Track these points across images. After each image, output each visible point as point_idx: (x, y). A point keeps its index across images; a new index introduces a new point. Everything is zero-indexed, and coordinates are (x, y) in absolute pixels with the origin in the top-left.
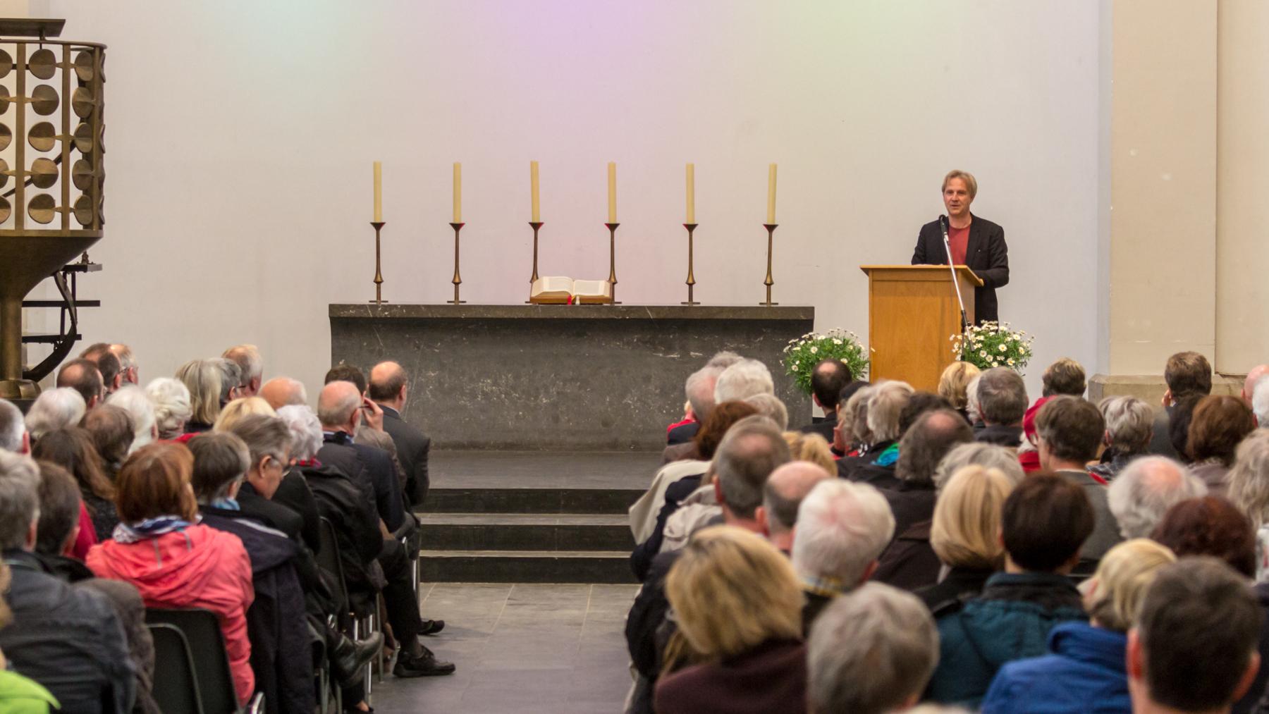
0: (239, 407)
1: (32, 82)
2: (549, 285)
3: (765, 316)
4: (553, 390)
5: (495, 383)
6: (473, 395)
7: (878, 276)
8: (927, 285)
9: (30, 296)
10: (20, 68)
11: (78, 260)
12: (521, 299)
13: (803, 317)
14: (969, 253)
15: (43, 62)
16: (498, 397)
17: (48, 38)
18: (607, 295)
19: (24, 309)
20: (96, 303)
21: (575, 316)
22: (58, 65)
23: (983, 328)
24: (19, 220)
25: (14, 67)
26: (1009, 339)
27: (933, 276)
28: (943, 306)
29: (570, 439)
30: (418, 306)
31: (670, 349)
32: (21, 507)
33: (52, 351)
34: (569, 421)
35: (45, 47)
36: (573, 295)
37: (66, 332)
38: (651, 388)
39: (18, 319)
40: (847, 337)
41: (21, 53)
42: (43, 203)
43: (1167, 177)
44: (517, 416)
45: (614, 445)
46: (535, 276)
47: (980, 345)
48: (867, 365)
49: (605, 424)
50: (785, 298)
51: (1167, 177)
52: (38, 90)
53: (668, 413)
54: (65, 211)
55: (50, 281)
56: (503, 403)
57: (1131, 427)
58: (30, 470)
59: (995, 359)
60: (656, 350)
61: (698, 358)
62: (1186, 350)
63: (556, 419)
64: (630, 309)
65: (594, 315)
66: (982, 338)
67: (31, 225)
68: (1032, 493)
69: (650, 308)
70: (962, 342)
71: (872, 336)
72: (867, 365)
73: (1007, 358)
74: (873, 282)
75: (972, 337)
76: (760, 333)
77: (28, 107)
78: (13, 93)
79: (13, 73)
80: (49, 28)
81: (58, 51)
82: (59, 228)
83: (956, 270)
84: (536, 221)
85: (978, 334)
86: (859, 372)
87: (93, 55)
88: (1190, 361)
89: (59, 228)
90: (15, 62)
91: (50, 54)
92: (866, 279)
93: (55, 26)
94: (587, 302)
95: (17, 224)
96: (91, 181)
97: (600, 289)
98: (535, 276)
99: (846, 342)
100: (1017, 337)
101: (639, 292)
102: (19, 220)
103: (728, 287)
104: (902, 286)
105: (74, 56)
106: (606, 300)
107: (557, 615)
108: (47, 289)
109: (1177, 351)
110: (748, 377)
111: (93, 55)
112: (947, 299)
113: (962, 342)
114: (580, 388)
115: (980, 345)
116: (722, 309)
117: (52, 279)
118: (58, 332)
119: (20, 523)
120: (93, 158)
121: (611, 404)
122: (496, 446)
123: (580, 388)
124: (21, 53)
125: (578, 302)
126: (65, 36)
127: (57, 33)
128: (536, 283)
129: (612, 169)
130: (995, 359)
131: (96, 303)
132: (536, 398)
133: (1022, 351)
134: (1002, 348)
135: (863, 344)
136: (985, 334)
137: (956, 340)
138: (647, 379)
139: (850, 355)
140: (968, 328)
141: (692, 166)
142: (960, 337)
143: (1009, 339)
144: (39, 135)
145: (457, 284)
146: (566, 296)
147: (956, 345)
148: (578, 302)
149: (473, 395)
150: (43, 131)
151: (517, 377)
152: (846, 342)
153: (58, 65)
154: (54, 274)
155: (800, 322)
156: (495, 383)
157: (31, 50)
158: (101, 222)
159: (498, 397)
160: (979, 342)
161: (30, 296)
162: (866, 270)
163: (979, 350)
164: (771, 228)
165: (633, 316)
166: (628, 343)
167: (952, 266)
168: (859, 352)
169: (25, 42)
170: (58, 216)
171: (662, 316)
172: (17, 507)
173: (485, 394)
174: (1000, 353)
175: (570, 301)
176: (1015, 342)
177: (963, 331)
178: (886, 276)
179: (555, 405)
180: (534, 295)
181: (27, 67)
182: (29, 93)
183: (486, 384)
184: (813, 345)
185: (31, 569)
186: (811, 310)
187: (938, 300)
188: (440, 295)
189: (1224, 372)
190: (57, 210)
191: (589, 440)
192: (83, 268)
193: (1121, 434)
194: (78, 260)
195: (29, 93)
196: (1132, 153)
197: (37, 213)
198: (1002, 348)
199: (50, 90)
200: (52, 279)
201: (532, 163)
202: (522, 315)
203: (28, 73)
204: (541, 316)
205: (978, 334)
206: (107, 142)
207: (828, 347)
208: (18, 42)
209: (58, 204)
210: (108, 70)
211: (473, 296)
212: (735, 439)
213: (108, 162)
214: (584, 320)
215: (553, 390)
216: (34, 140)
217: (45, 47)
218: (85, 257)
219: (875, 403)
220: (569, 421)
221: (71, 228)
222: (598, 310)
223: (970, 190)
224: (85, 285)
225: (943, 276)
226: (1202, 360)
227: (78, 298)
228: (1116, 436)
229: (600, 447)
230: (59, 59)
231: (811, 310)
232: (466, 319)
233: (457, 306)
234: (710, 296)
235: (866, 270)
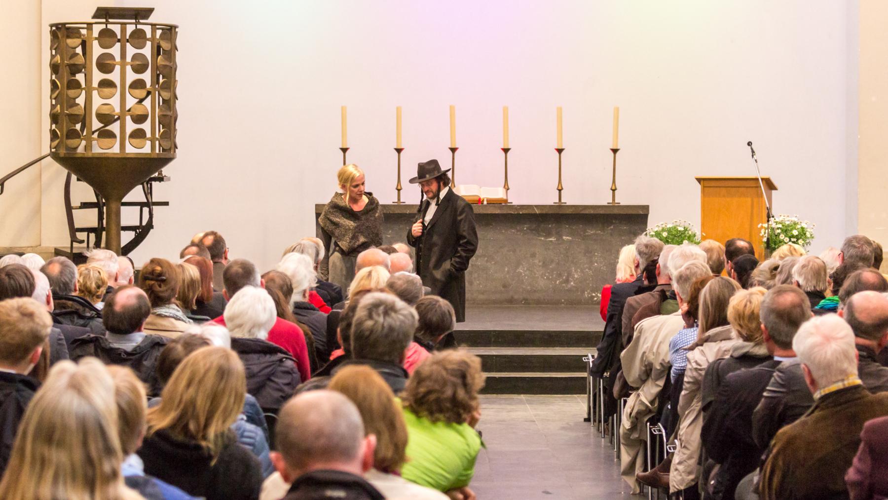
0: (370, 274)
1: (131, 51)
3: (616, 211)
9: (124, 200)
10: (123, 41)
11: (156, 174)
13: (641, 212)
14: (217, 248)
15: (138, 37)
17: (141, 21)
19: (122, 208)
20: (166, 204)
21: (485, 212)
22: (148, 40)
24: (122, 146)
25: (119, 41)
26: (799, 226)
29: (481, 297)
31: (549, 235)
32: (401, 336)
33: (133, 237)
35: (139, 27)
37: (144, 224)
38: (536, 261)
39: (118, 214)
40: (686, 226)
41: (123, 31)
42: (138, 134)
45: (511, 301)
47: (779, 231)
49: (505, 286)
50: (625, 199)
52: (135, 57)
53: (548, 278)
54: (153, 141)
55: (139, 188)
60: (540, 235)
61: (568, 241)
65: (498, 212)
66: (780, 226)
67: (130, 150)
69: (536, 206)
70: (768, 228)
71: (703, 225)
74: (704, 188)
77: (129, 68)
78: (118, 58)
79: (118, 45)
80: (141, 14)
81: (148, 30)
82: (149, 151)
87: (170, 31)
89: (149, 151)
90: (119, 37)
91: (142, 32)
92: (698, 187)
93: (145, 13)
94: (491, 202)
95: (121, 149)
96: (168, 122)
97: (499, 193)
99: (686, 229)
100: (804, 225)
102: (122, 146)
104: (724, 190)
105: (159, 32)
107: (514, 415)
108: (137, 194)
111: (170, 31)
112: (755, 200)
114: (487, 261)
115: (779, 231)
117: (141, 186)
118: (138, 224)
119: (398, 346)
120: (169, 104)
121: (508, 272)
123: (487, 261)
124: (123, 31)
125: (485, 203)
126: (152, 19)
127: (147, 17)
129: (617, 110)
131: (166, 204)
133: (808, 235)
137: (762, 227)
138: (533, 255)
143: (799, 226)
144: (136, 88)
145: (399, 190)
146: (477, 199)
147: (763, 231)
148: (485, 203)
150: (138, 84)
152: (686, 229)
153: (148, 40)
154: (142, 184)
157: (130, 29)
158: (176, 147)
161: (124, 200)
163: (779, 234)
165: (525, 212)
168: (695, 235)
169: (126, 24)
170: (149, 143)
171: (544, 212)
172: (398, 335)
174: (793, 236)
175: (480, 201)
177: (768, 221)
178: (713, 184)
181: (128, 41)
182: (129, 59)
185: (398, 376)
186: (646, 208)
187: (749, 200)
188: (550, 199)
190: (148, 139)
191: (493, 297)
192: (160, 179)
194: (156, 174)
195: (129, 59)
197: (135, 141)
198: (795, 233)
199: (143, 56)
200: (141, 186)
201: (397, 108)
203: (128, 44)
206: (179, 92)
208: (122, 24)
209: (149, 135)
210: (179, 42)
211: (571, 199)
213: (179, 105)
214: (604, 215)
216: (133, 91)
217: (139, 27)
218: (160, 173)
221: (127, 151)
222: (501, 208)
224: (159, 191)
229: (501, 302)
230: (149, 35)
231: (646, 208)
233: (560, 206)
234: (518, 198)
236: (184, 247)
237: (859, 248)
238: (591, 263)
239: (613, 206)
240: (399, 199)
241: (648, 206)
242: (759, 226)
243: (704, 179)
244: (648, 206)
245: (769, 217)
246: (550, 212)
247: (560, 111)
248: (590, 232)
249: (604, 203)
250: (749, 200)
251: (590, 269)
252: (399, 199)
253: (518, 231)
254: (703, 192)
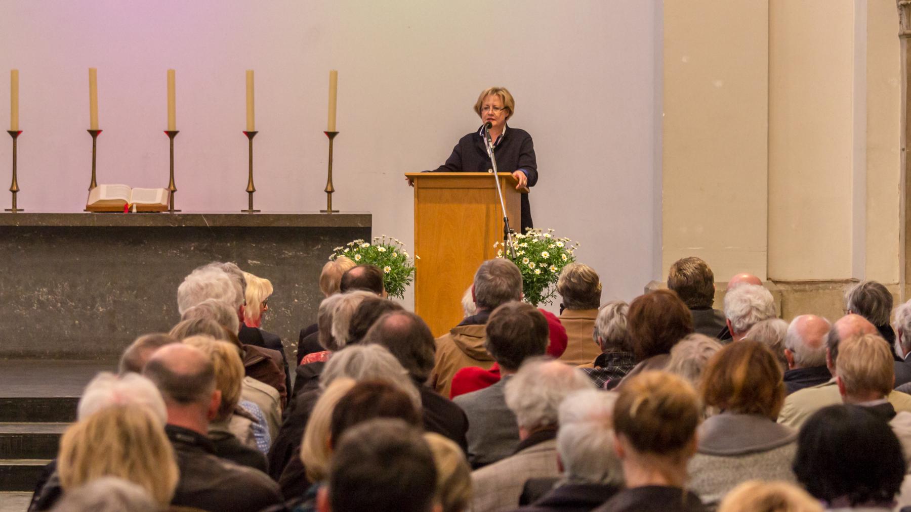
2: (106, 193)
3: (323, 224)
4: (110, 299)
5: (51, 292)
6: (28, 304)
7: (423, 183)
8: (471, 191)
12: (80, 209)
16: (54, 306)
18: (165, 203)
23: (528, 235)
26: (553, 246)
27: (472, 183)
28: (488, 216)
30: (200, 215)
34: (125, 330)
36: (130, 203)
40: (392, 245)
43: (718, 84)
44: (74, 324)
46: (94, 184)
47: (523, 252)
48: (412, 273)
50: (343, 206)
51: (718, 84)
56: (60, 311)
57: (621, 329)
58: (375, 349)
59: (537, 267)
62: (685, 256)
63: (113, 328)
64: (186, 217)
65: (150, 223)
66: (525, 245)
68: (360, 399)
69: (206, 216)
70: (506, 248)
71: (417, 243)
72: (412, 273)
73: (549, 265)
75: (515, 244)
76: (317, 241)
83: (500, 177)
84: (94, 129)
85: (523, 241)
86: (403, 280)
88: (690, 270)
94: (145, 210)
97: (158, 197)
98: (94, 184)
99: (390, 250)
100: (560, 244)
101: (274, 202)
103: (209, 193)
104: (447, 193)
106: (165, 208)
109: (677, 259)
110: (202, 284)
112: (492, 206)
113: (506, 248)
114: (136, 297)
115: (523, 252)
116: (228, 216)
122: (52, 356)
125: (134, 210)
128: (93, 191)
129: (334, 76)
130: (537, 267)
132: (93, 306)
134: (545, 255)
135: (409, 253)
136: (528, 241)
137: (499, 247)
139: (394, 263)
140: (509, 235)
141: (252, 73)
142: (503, 244)
143: (553, 246)
145: (14, 192)
146: (123, 204)
148: (134, 210)
149: (28, 304)
151: (73, 286)
152: (390, 250)
155: (356, 229)
156: (51, 292)
159: (54, 306)
160: (524, 249)
162: (411, 179)
163: (522, 257)
164: (172, 134)
165: (189, 224)
166: (186, 252)
167: (496, 174)
168: (404, 259)
171: (218, 224)
173: (41, 303)
175: (127, 209)
176: (559, 249)
177: (506, 238)
179: (112, 314)
180: (90, 203)
183: (42, 293)
184: (358, 252)
187: (483, 207)
188: (236, 206)
189: (777, 278)
193: (612, 338)
196: (684, 60)
201: (12, 72)
202: (77, 223)
204: (97, 224)
205: (523, 241)
207: (372, 254)
212: (137, 350)
215: (110, 299)
219: (338, 309)
220: (125, 330)
223: (508, 110)
225: (487, 184)
226: (702, 268)
227: (11, 207)
228: (608, 339)
231: (369, 217)
232: (20, 227)
233: (251, 214)
234: (192, 203)
235: (411, 179)
236: (829, 278)
237: (491, 281)
238: (290, 298)
239: (329, 215)
240: (14, 205)
241: (370, 216)
242: (495, 246)
243: (419, 177)
244: (370, 216)
245: (506, 233)
246: (228, 224)
247: (171, 76)
248: (288, 254)
249: (238, 211)
250: (483, 207)
251: (287, 308)
252: (14, 205)
253: (181, 252)
254: (417, 196)
